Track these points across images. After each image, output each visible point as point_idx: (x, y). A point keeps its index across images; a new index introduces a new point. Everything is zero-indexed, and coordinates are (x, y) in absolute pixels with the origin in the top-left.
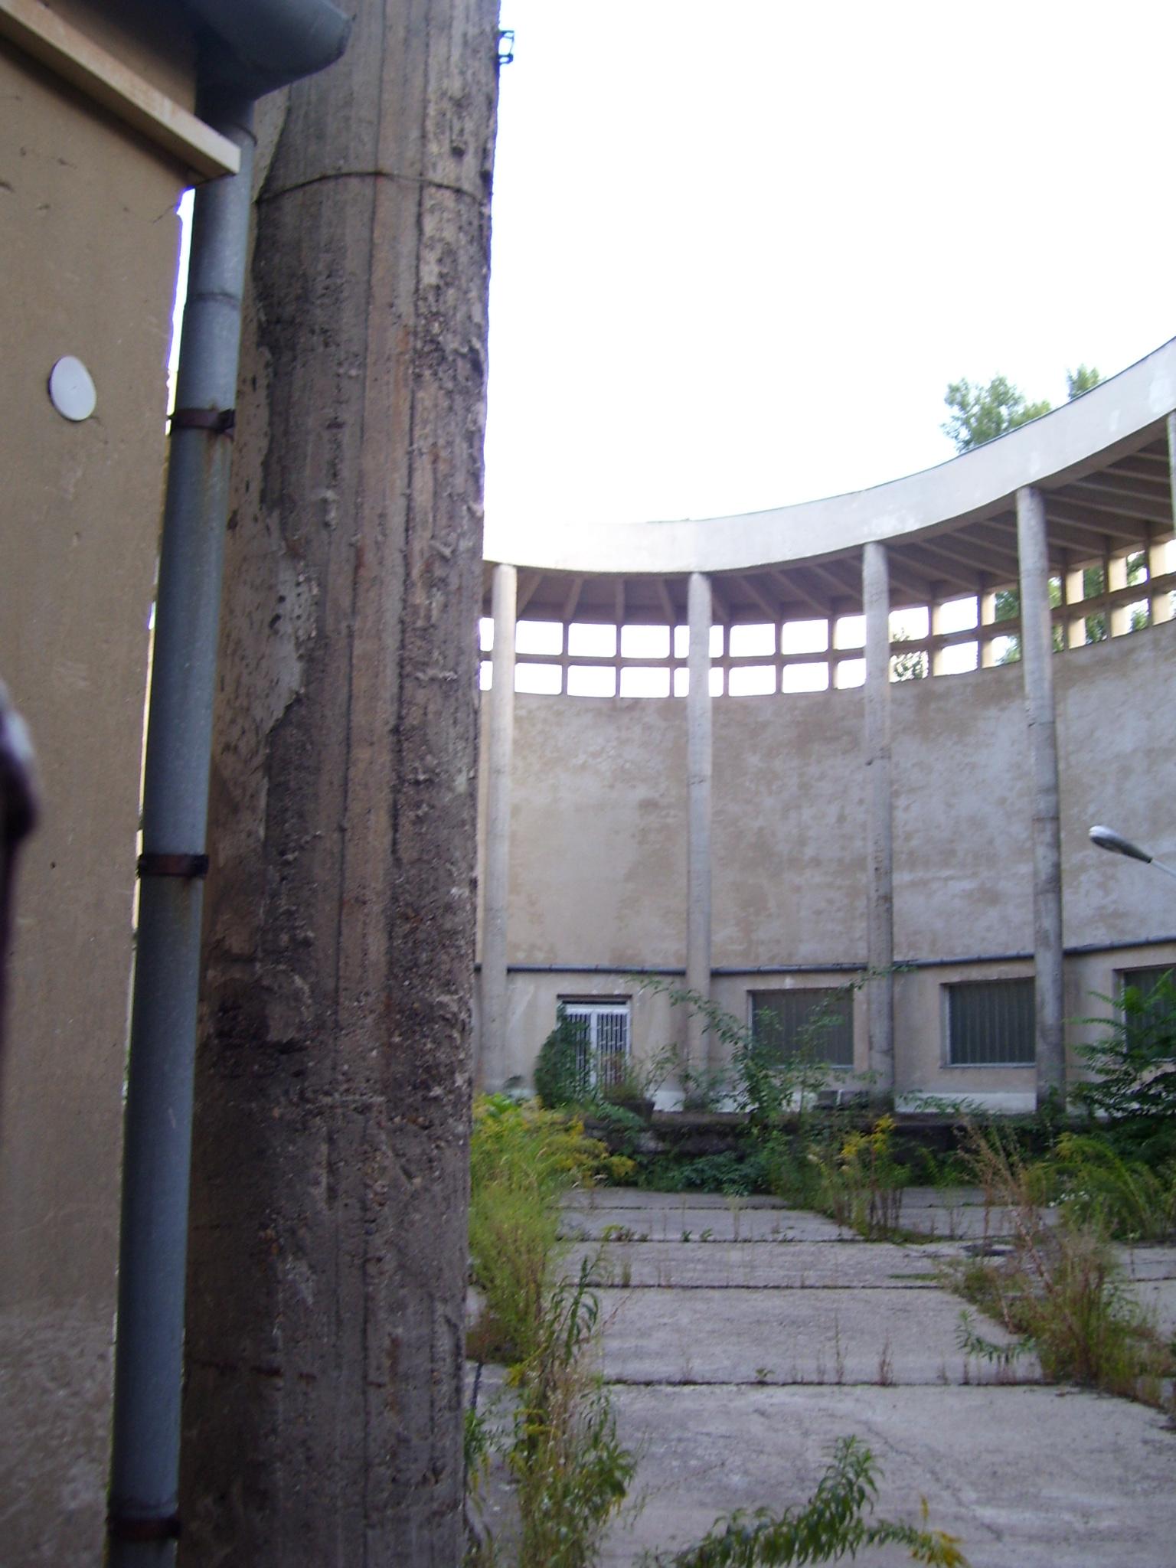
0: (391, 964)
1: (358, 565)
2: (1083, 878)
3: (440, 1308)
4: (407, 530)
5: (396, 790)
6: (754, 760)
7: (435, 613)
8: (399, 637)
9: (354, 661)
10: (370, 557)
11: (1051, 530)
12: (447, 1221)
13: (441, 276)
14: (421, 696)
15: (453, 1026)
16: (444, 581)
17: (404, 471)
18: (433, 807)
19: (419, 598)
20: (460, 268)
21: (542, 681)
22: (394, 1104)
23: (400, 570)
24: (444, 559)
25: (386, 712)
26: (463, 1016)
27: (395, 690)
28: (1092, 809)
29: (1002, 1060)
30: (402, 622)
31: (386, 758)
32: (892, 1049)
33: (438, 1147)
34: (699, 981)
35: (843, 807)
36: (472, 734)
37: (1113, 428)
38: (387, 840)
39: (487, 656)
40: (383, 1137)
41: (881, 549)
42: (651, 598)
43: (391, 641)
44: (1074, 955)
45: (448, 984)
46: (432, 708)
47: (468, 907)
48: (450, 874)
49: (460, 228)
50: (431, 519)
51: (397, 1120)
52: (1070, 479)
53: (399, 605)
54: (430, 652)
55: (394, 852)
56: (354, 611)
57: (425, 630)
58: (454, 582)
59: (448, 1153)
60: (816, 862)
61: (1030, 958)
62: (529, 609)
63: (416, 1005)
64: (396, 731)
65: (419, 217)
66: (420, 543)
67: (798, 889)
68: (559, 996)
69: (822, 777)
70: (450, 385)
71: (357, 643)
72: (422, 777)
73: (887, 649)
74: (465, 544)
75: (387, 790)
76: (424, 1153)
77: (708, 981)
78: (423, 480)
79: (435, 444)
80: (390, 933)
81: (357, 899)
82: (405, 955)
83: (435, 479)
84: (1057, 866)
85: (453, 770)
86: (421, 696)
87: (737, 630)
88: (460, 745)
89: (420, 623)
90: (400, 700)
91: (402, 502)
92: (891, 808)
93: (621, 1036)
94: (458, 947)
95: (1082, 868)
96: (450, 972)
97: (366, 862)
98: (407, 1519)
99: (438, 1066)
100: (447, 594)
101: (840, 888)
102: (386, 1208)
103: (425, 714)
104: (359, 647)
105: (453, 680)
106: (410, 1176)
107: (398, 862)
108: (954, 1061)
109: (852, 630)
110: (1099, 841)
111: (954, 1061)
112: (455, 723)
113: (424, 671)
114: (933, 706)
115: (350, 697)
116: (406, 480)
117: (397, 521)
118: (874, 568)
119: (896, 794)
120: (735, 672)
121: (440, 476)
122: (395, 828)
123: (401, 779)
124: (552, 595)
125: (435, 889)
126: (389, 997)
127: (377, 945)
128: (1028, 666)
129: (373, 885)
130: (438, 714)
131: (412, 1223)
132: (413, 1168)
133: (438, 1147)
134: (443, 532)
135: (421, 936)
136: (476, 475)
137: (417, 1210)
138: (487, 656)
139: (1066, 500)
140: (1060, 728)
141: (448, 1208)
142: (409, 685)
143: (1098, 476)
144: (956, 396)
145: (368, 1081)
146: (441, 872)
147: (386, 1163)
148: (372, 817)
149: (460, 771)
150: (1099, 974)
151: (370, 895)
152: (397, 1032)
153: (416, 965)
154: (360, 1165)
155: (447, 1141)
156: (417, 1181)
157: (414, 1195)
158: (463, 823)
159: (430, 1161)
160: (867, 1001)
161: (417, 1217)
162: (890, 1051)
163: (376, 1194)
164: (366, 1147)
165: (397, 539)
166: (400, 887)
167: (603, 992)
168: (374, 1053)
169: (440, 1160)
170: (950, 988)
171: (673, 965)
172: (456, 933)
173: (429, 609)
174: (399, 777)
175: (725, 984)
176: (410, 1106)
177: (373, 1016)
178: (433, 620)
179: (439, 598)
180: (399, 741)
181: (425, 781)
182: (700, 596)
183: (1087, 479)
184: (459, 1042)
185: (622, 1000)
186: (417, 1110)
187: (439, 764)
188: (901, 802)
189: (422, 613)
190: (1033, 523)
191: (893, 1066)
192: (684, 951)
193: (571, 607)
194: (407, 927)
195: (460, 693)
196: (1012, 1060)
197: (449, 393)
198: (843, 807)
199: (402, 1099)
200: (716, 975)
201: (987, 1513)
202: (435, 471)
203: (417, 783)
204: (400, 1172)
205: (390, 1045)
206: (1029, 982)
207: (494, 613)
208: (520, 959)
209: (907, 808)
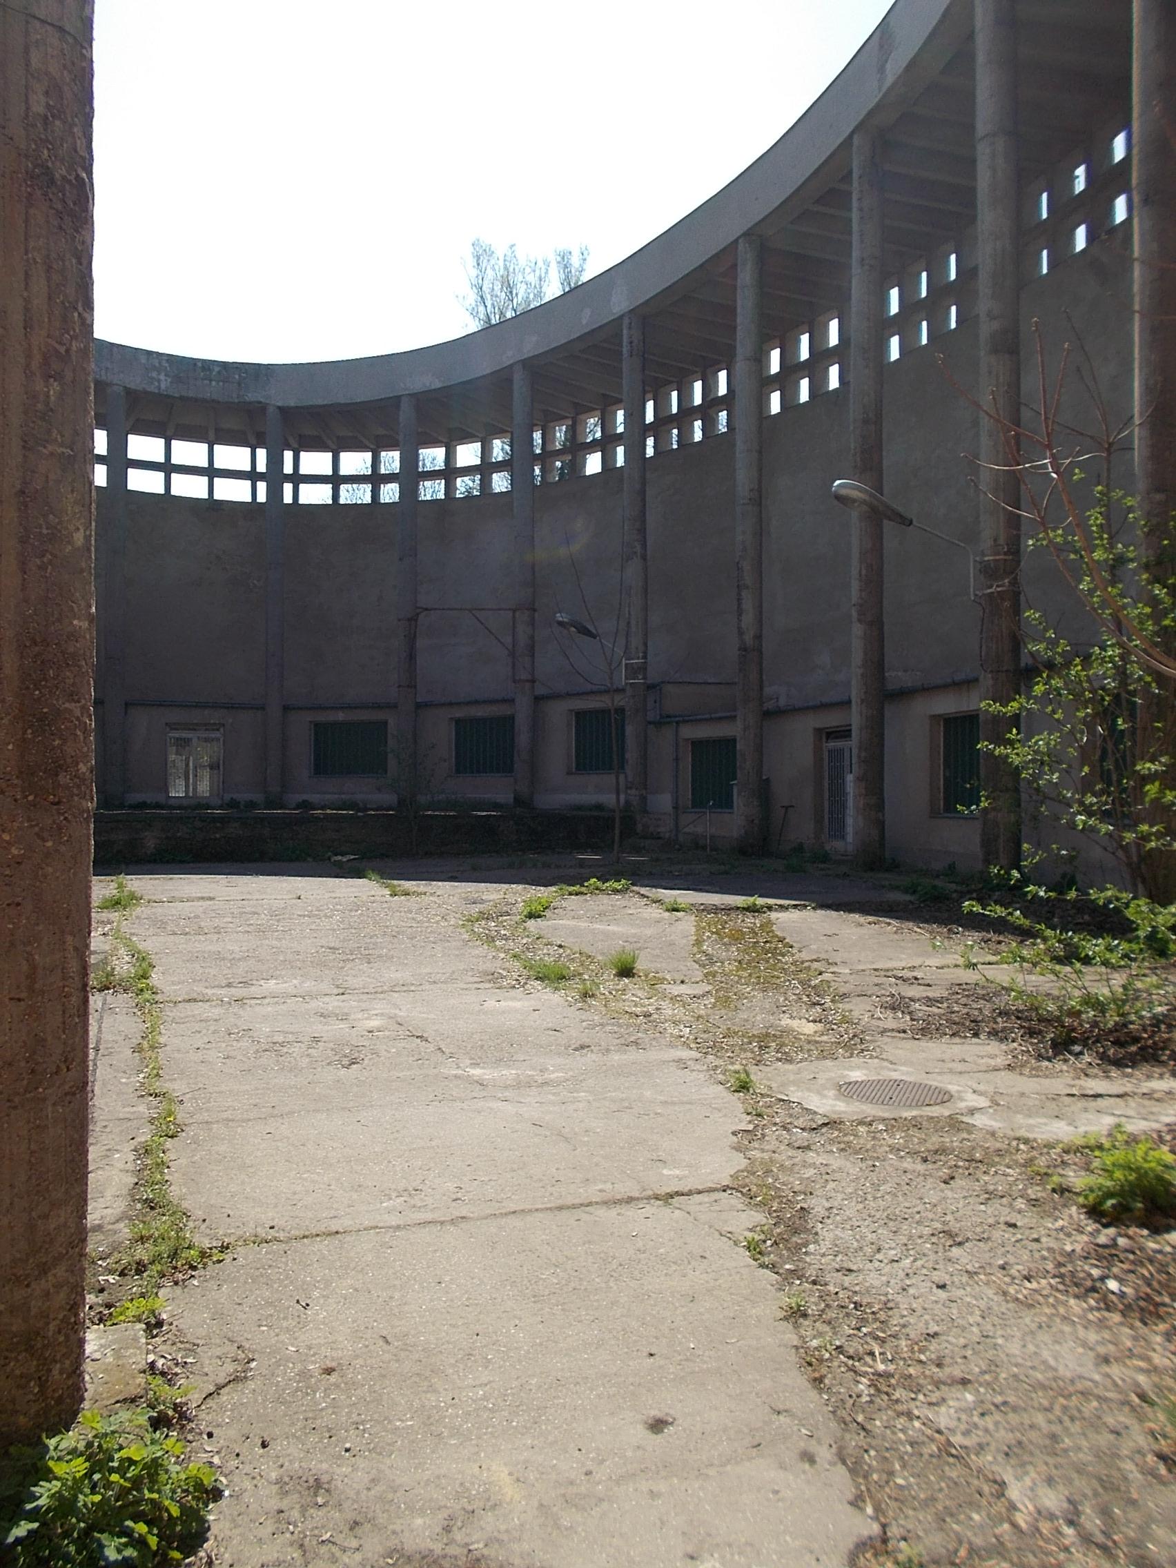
3: (69, 939)
5: (23, 541)
13: (48, 106)
18: (56, 556)
19: (39, 385)
20: (65, 102)
36: (74, 966)
37: (584, 322)
48: (72, 609)
49: (65, 67)
54: (49, 432)
58: (69, 375)
61: (512, 701)
65: (27, 51)
70: (59, 206)
76: (54, 822)
79: (48, 256)
84: (532, 637)
85: (72, 528)
96: (73, 685)
98: (44, 1100)
103: (47, 481)
105: (70, 456)
111: (458, 771)
112: (72, 491)
118: (406, 413)
120: (303, 488)
125: (59, 620)
131: (45, 876)
132: (45, 835)
133: (66, 819)
144: (481, 255)
150: (559, 715)
158: (82, 571)
161: (50, 870)
168: (10, 747)
178: (51, 405)
189: (42, 398)
193: (169, 433)
197: (59, 215)
201: (476, 1072)
202: (49, 279)
205: (24, 740)
206: (512, 718)
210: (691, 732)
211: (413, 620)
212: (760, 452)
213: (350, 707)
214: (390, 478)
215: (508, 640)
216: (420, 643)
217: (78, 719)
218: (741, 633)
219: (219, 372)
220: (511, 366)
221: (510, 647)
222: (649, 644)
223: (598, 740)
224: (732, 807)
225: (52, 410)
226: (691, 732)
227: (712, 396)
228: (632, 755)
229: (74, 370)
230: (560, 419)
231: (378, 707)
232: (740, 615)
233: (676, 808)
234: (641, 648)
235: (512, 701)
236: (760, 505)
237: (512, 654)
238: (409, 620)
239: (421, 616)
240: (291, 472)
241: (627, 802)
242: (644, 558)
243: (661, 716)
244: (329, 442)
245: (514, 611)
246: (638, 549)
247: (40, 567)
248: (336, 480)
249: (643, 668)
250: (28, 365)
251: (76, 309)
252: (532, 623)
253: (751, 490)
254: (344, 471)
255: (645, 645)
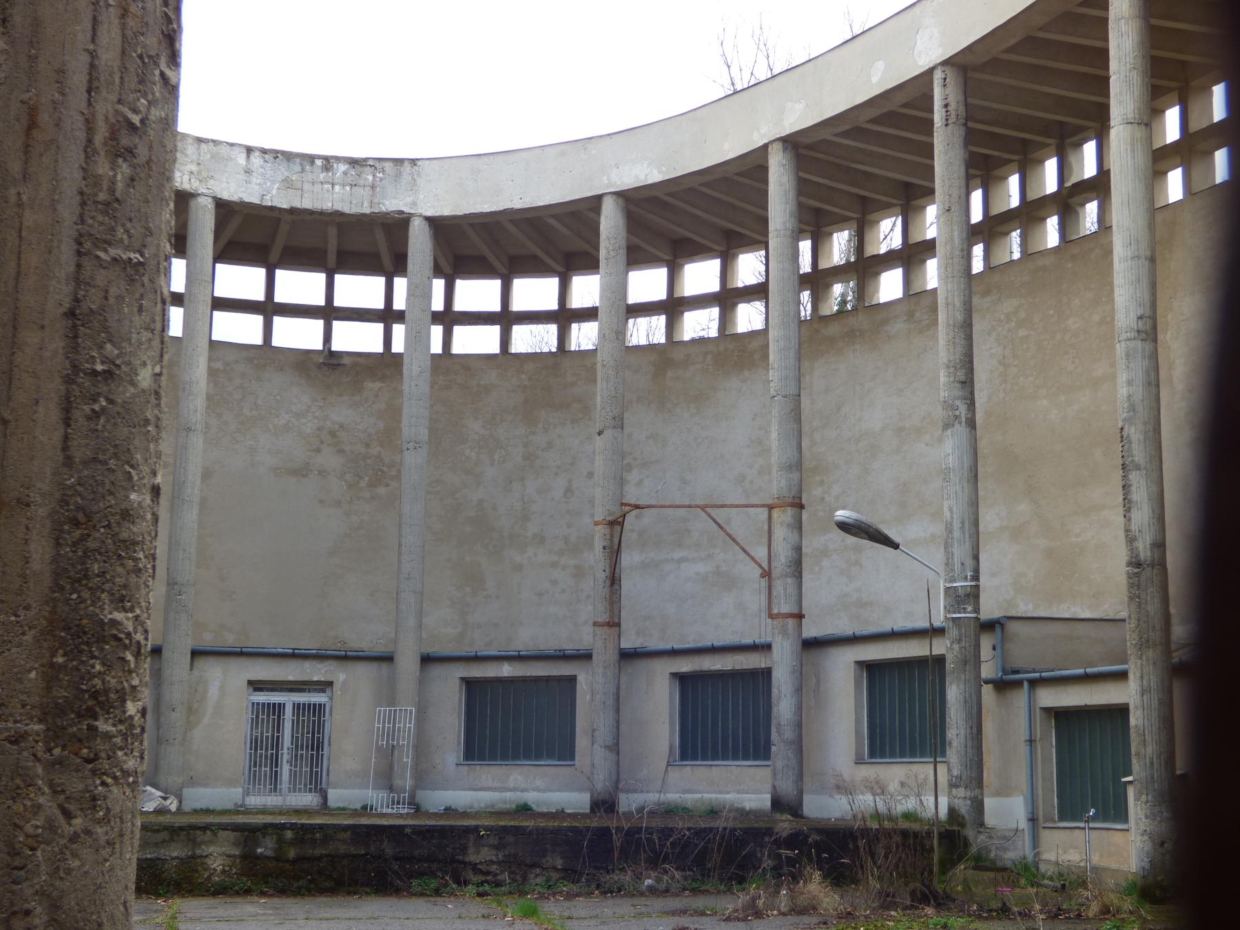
0: (57, 575)
1: (32, 125)
2: (826, 563)
4: (89, 91)
5: (69, 380)
6: (475, 427)
7: (120, 185)
8: (78, 210)
9: (24, 234)
10: (44, 118)
11: (803, 187)
12: (111, 869)
14: (101, 277)
15: (126, 647)
16: (130, 152)
17: (87, 24)
18: (111, 401)
19: (102, 167)
21: (240, 329)
22: (55, 735)
23: (81, 135)
24: (132, 127)
25: (60, 293)
26: (139, 637)
27: (72, 269)
28: (836, 490)
29: (735, 758)
30: (81, 193)
31: (57, 344)
32: (617, 744)
33: (104, 784)
34: (408, 663)
35: (570, 481)
36: (158, 326)
37: (875, 79)
38: (58, 435)
39: (178, 299)
40: (40, 770)
41: (621, 201)
42: (368, 242)
43: (68, 211)
44: (812, 645)
45: (122, 599)
46: (113, 291)
47: (149, 516)
48: (130, 477)
50: (117, 80)
51: (57, 751)
52: (826, 134)
53: (78, 175)
54: (112, 230)
55: (65, 448)
56: (26, 176)
57: (107, 204)
58: (142, 152)
59: (115, 789)
60: (540, 539)
61: (767, 647)
62: (234, 248)
63: (84, 622)
64: (71, 314)
66: (104, 107)
67: (519, 568)
68: (250, 683)
69: (550, 445)
71: (27, 213)
72: (99, 367)
73: (623, 310)
74: (155, 113)
75: (58, 380)
77: (418, 667)
78: (110, 35)
80: (57, 539)
81: (19, 501)
82: (73, 566)
83: (124, 36)
84: (798, 549)
86: (101, 277)
87: (461, 285)
88: (146, 335)
89: (102, 196)
90: (78, 279)
91: (85, 58)
92: (622, 482)
93: (318, 727)
94: (136, 560)
95: (825, 553)
96: (125, 587)
97: (32, 459)
99: (106, 691)
100: (134, 166)
101: (564, 568)
102: (39, 853)
104: (29, 218)
105: (140, 263)
106: (68, 816)
107: (68, 461)
108: (684, 756)
109: (586, 290)
110: (844, 526)
111: (684, 756)
112: (140, 310)
113: (106, 251)
114: (670, 374)
115: (18, 273)
116: (89, 35)
117: (78, 80)
118: (610, 222)
119: (629, 468)
121: (129, 33)
122: (67, 422)
123: (75, 367)
124: (257, 235)
126: (53, 612)
127: (40, 551)
128: (772, 334)
129: (39, 485)
130: (120, 298)
131: (69, 871)
132: (72, 807)
133: (104, 784)
134: (132, 97)
135: (91, 544)
136: (171, 39)
137: (75, 855)
138: (178, 299)
139: (820, 156)
140: (805, 402)
141: (113, 853)
142: (87, 263)
143: (857, 132)
145: (23, 706)
146: (119, 475)
147: (41, 800)
148: (41, 409)
149: (144, 364)
150: (841, 670)
151: (35, 497)
152: (61, 651)
153: (86, 576)
154: (10, 802)
155: (115, 778)
156: (78, 822)
157: (74, 838)
159: (94, 799)
160: (591, 685)
162: (615, 748)
163: (27, 836)
164: (18, 781)
165: (78, 99)
166: (70, 487)
167: (300, 679)
168: (33, 675)
169: (105, 798)
170: (683, 679)
171: (381, 648)
172: (135, 543)
173: (113, 182)
174: (74, 366)
175: (437, 670)
176: (74, 735)
177: (33, 632)
179: (124, 169)
180: (75, 326)
181: (104, 371)
182: (420, 244)
183: (845, 134)
184: (132, 666)
185: (324, 686)
186: (80, 740)
187: (118, 356)
188: (633, 476)
190: (785, 179)
191: (618, 763)
192: (393, 635)
193: (275, 255)
194: (77, 533)
195: (146, 279)
196: (746, 758)
198: (570, 481)
199: (64, 728)
200: (427, 660)
202: (123, 27)
203: (95, 373)
204: (57, 812)
206: (767, 673)
207: (189, 251)
208: (208, 640)
209: (640, 483)
210: (1051, 698)
211: (616, 524)
212: (1152, 260)
213: (520, 658)
214: (589, 314)
215: (761, 553)
216: (627, 559)
217: (129, 635)
218: (1131, 540)
219: (345, 173)
220: (765, 146)
221: (765, 565)
222: (982, 557)
223: (903, 700)
224: (1126, 820)
225: (117, 200)
226: (1051, 698)
227: (1074, 179)
228: (956, 730)
229: (151, 148)
230: (839, 222)
231: (563, 657)
232: (1128, 510)
233: (1033, 820)
234: (969, 563)
235: (767, 647)
236: (1155, 340)
237: (767, 574)
238: (612, 524)
239: (630, 520)
240: (440, 351)
241: (952, 811)
242: (971, 424)
243: (1005, 672)
244: (497, 264)
245: (771, 508)
246: (963, 410)
247: (89, 418)
248: (506, 318)
249: (973, 595)
250: (90, 141)
251: (157, 64)
252: (798, 526)
253: (1140, 318)
254: (517, 305)
255: (976, 558)
